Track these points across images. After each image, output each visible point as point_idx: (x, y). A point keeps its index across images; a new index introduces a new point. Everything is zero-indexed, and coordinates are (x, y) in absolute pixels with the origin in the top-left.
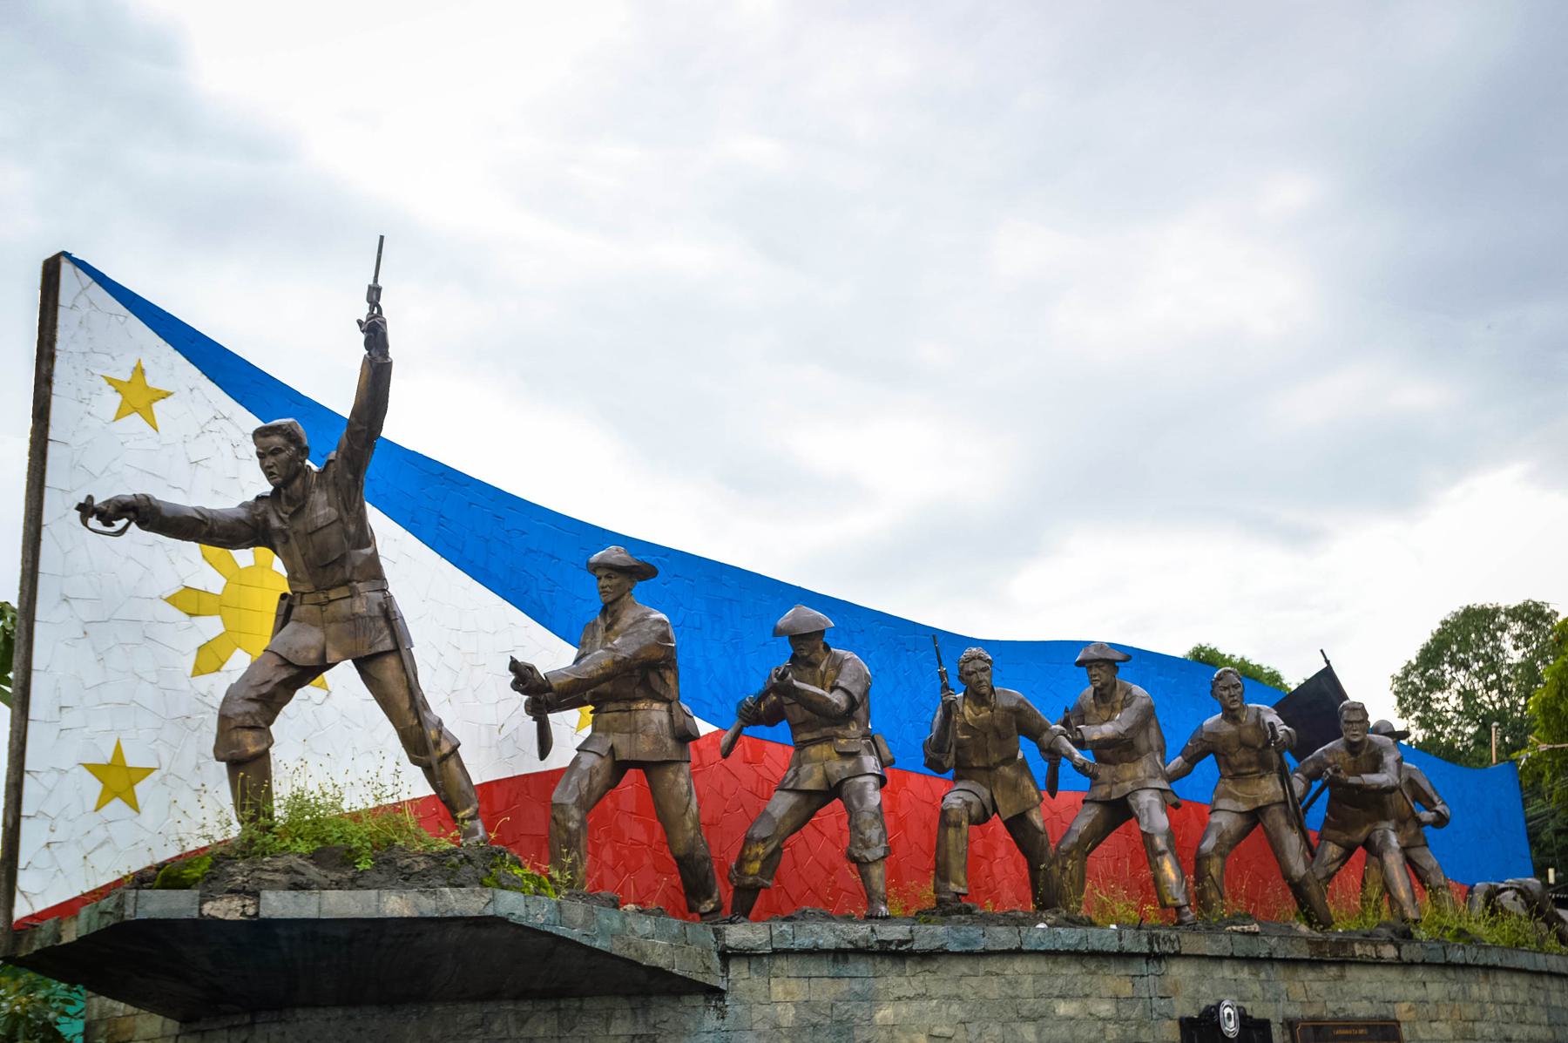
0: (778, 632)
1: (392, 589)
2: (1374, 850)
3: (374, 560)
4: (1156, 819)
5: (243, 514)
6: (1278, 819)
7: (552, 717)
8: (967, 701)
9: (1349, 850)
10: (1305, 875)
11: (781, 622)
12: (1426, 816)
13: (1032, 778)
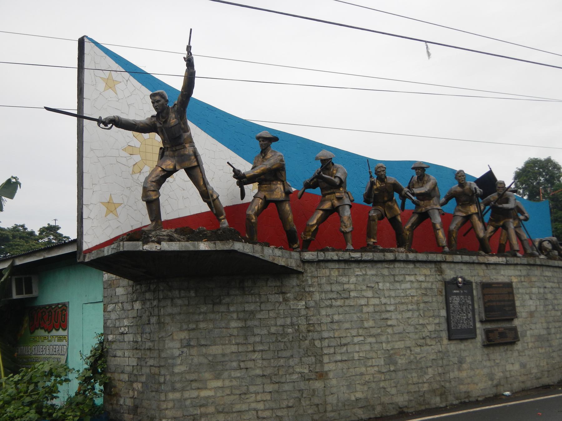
0: (317, 159)
1: (197, 145)
2: (505, 227)
3: (190, 137)
4: (437, 220)
5: (148, 122)
6: (475, 218)
7: (245, 186)
8: (377, 181)
9: (496, 228)
10: (484, 236)
11: (318, 155)
12: (522, 217)
13: (397, 205)
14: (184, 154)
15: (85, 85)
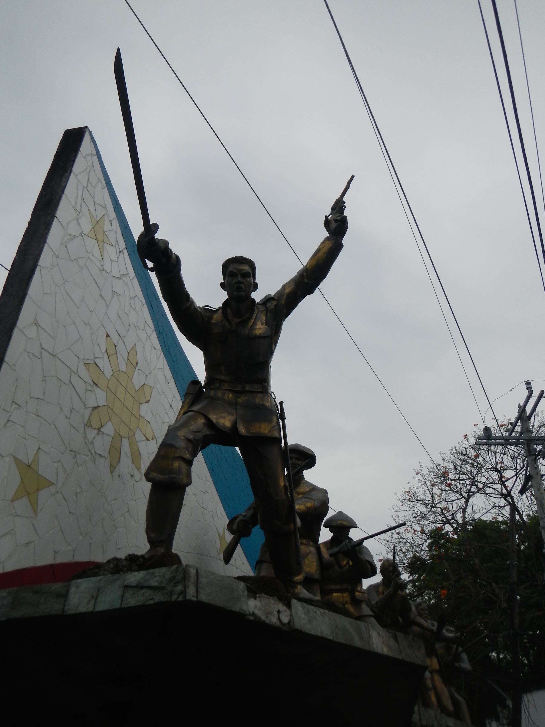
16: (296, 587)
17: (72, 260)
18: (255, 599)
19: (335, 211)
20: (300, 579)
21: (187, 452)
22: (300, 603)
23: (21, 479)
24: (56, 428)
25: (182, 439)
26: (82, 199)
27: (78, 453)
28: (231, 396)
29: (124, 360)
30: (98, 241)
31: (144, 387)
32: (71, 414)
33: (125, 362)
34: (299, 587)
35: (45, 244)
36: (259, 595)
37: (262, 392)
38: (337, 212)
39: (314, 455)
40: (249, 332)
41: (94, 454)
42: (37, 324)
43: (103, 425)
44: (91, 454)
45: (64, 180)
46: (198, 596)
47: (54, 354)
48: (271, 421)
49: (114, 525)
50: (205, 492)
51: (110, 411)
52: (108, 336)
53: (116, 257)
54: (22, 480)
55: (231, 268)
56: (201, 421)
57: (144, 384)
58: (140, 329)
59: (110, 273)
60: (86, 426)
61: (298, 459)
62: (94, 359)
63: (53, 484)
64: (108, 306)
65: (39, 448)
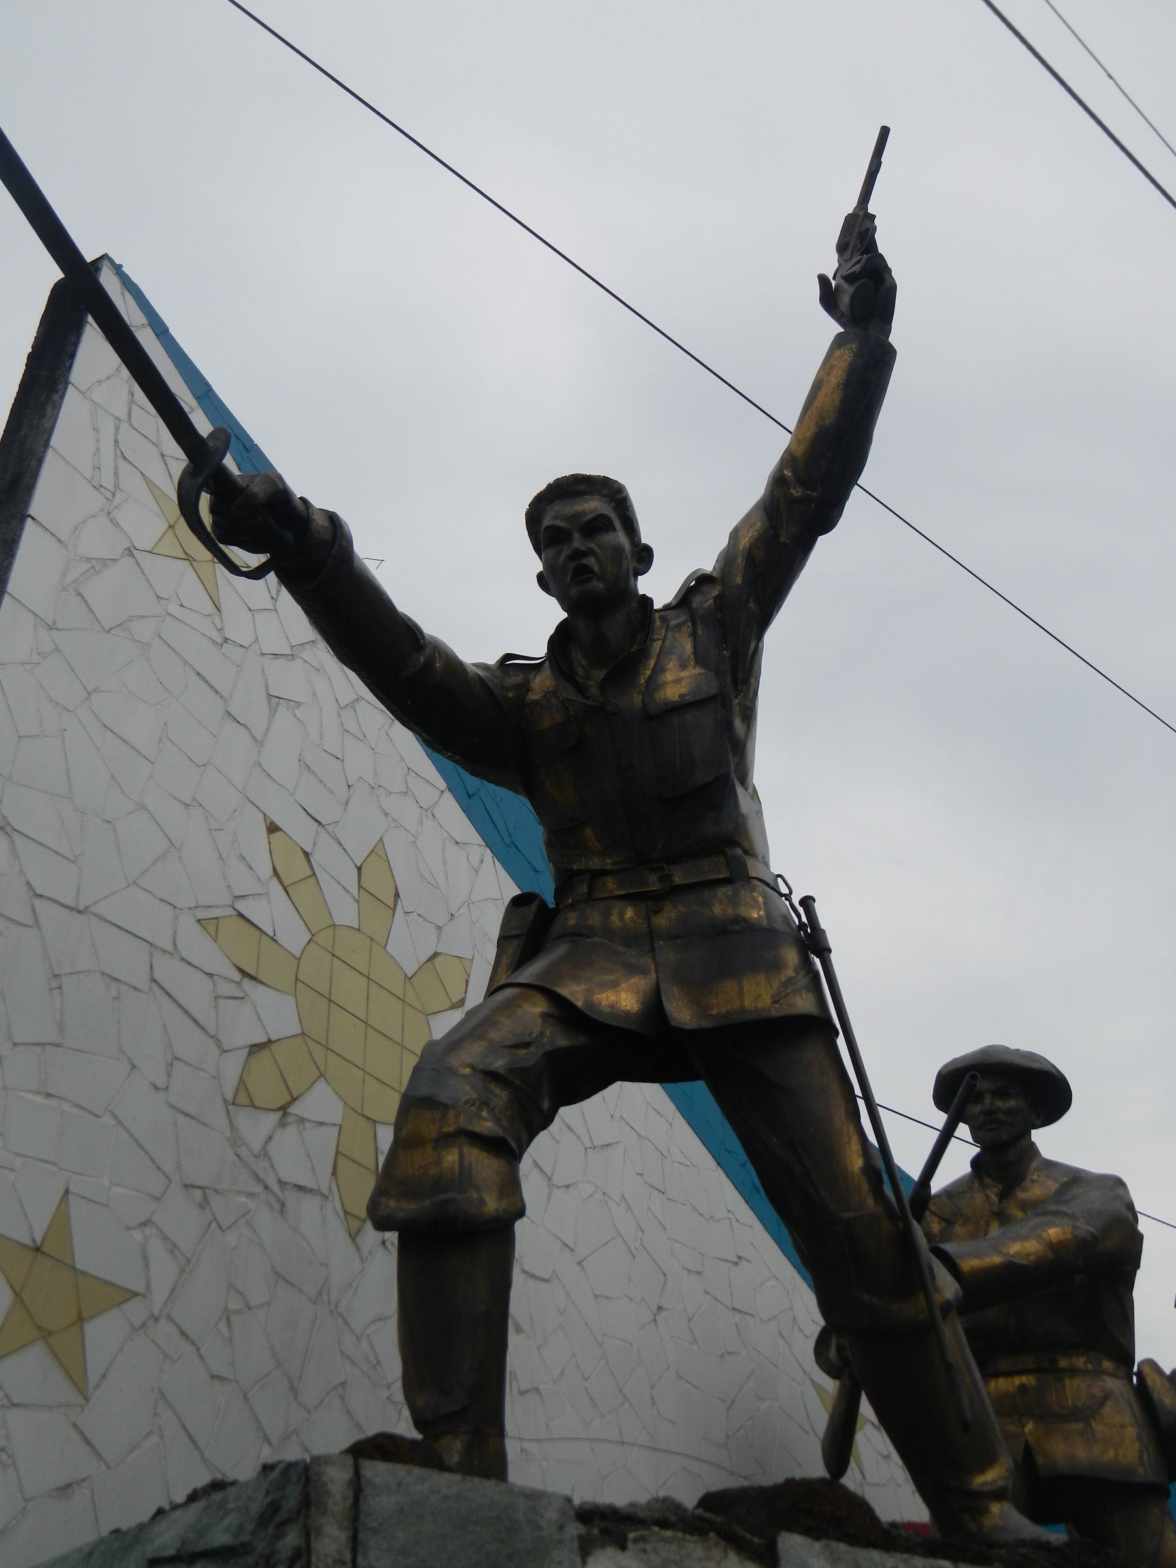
14: (738, 920)
15: (50, 458)
16: (985, 1511)
17: (107, 628)
18: (623, 1548)
19: (848, 254)
20: (993, 1481)
21: (485, 1114)
22: (818, 1546)
23: (14, 1291)
24: (120, 1123)
25: (464, 1076)
26: (116, 454)
27: (216, 1191)
28: (629, 913)
29: (348, 892)
30: (194, 564)
31: (437, 961)
32: (169, 1076)
33: (353, 896)
34: (995, 1508)
35: (4, 596)
36: (638, 1533)
37: (728, 881)
38: (852, 253)
39: (1053, 1071)
40: (643, 701)
41: (275, 1187)
42: (8, 829)
43: (295, 1095)
44: (266, 1187)
45: (51, 414)
46: (359, 1558)
47: (81, 908)
48: (776, 966)
49: (388, 1398)
50: (735, 1259)
51: (318, 1052)
52: (273, 828)
53: (269, 596)
54: (17, 1294)
55: (547, 521)
56: (537, 1007)
57: (436, 955)
58: (390, 793)
59: (250, 645)
60: (233, 1104)
61: (1000, 1093)
62: (233, 903)
63: (136, 1294)
64: (259, 743)
65: (67, 1192)
